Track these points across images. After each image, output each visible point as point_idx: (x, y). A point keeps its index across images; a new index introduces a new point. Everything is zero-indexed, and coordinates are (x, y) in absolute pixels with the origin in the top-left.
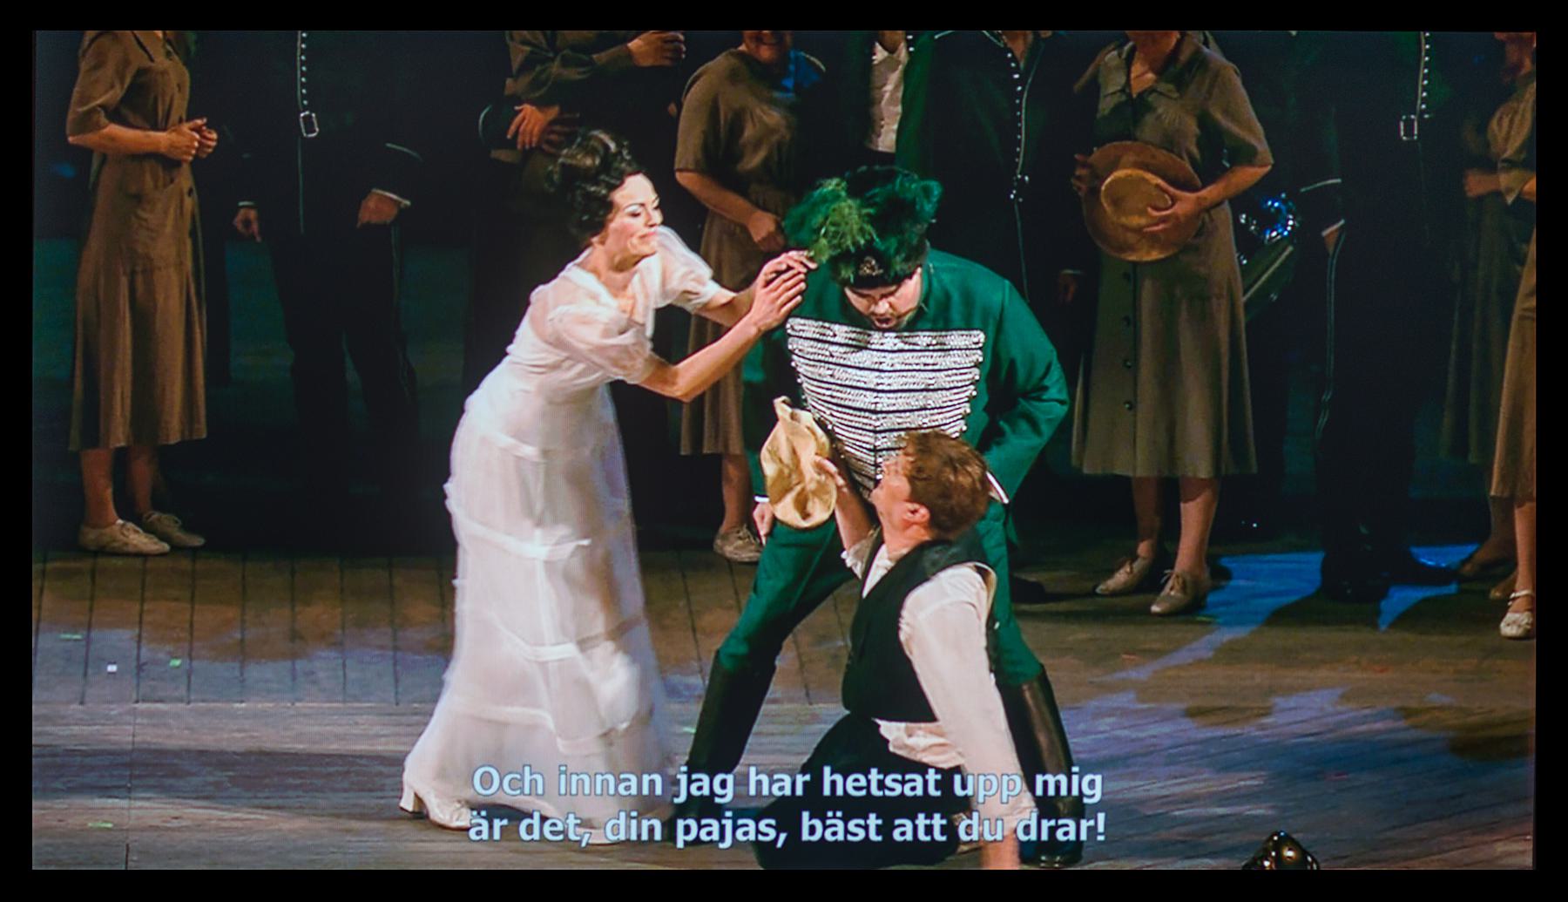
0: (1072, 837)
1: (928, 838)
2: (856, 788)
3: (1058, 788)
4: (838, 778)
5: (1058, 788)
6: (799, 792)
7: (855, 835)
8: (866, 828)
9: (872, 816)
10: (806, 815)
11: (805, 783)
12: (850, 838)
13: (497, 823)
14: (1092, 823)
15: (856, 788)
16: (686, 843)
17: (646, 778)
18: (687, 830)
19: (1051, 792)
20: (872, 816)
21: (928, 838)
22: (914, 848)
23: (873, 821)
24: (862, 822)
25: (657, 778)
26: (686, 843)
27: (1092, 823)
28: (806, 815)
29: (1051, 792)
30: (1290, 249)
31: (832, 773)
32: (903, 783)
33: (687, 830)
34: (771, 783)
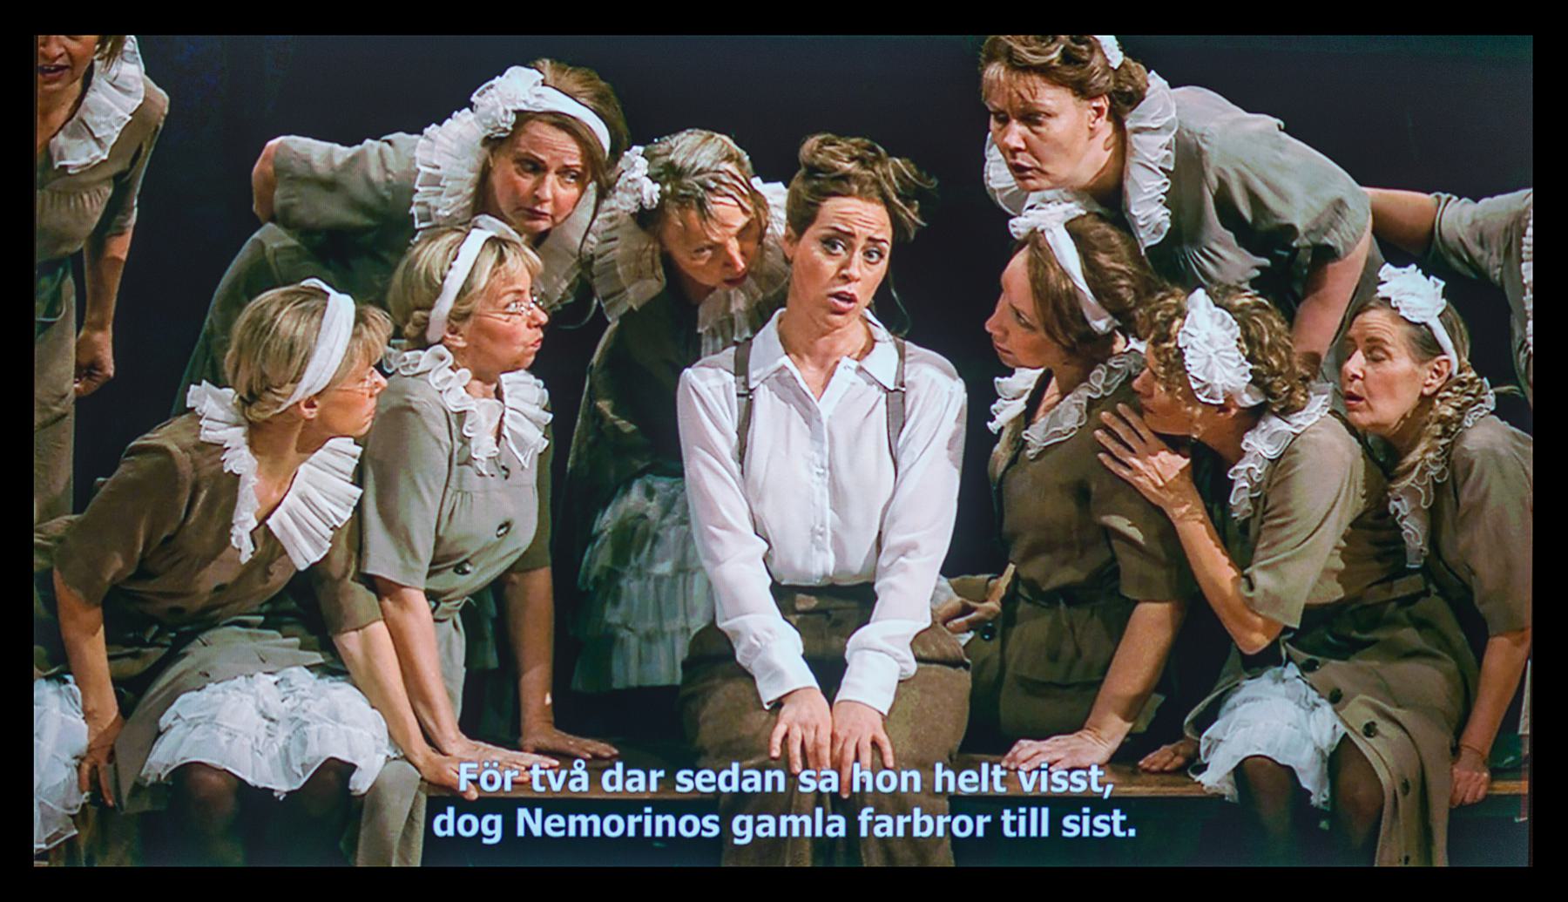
0: (772, 833)
1: (1123, 834)
2: (555, 829)
3: (863, 785)
4: (950, 775)
5: (863, 785)
6: (980, 833)
7: (1101, 831)
8: (1111, 823)
9: (1117, 812)
10: (939, 766)
11: (986, 824)
12: (1095, 834)
13: (654, 775)
14: (908, 819)
15: (555, 829)
16: (445, 813)
17: (905, 775)
18: (728, 781)
19: (584, 833)
20: (1117, 812)
21: (1123, 834)
22: (1028, 843)
23: (1117, 817)
24: (1107, 818)
25: (780, 775)
26: (445, 813)
27: (908, 819)
28: (939, 766)
29: (584, 833)
30: (1286, 254)
31: (944, 769)
32: (817, 779)
33: (728, 781)
34: (756, 823)
